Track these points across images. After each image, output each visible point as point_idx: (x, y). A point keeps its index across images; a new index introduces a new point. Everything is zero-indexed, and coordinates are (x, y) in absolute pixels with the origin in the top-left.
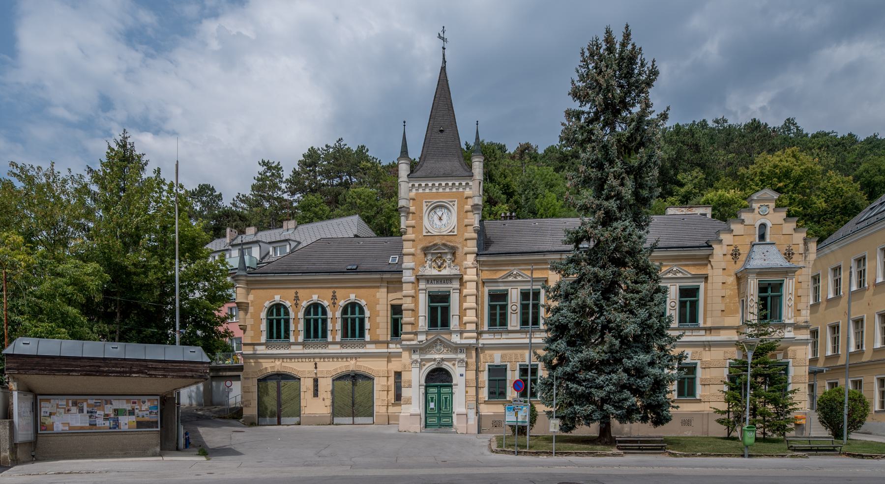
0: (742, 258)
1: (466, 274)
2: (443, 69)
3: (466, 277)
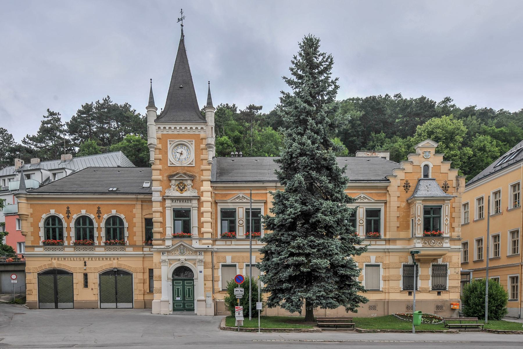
0: (412, 189)
3: (203, 199)
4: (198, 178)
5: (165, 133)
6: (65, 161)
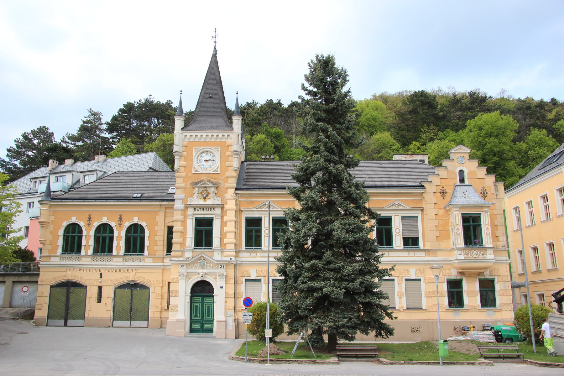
0: (448, 195)
1: (226, 204)
2: (214, 56)
3: (226, 207)
4: (222, 186)
5: (192, 140)
6: (98, 162)
